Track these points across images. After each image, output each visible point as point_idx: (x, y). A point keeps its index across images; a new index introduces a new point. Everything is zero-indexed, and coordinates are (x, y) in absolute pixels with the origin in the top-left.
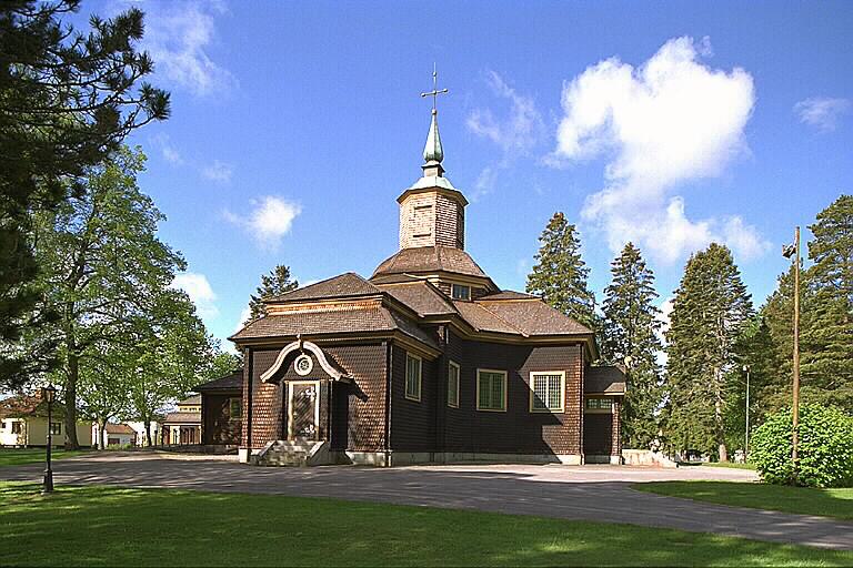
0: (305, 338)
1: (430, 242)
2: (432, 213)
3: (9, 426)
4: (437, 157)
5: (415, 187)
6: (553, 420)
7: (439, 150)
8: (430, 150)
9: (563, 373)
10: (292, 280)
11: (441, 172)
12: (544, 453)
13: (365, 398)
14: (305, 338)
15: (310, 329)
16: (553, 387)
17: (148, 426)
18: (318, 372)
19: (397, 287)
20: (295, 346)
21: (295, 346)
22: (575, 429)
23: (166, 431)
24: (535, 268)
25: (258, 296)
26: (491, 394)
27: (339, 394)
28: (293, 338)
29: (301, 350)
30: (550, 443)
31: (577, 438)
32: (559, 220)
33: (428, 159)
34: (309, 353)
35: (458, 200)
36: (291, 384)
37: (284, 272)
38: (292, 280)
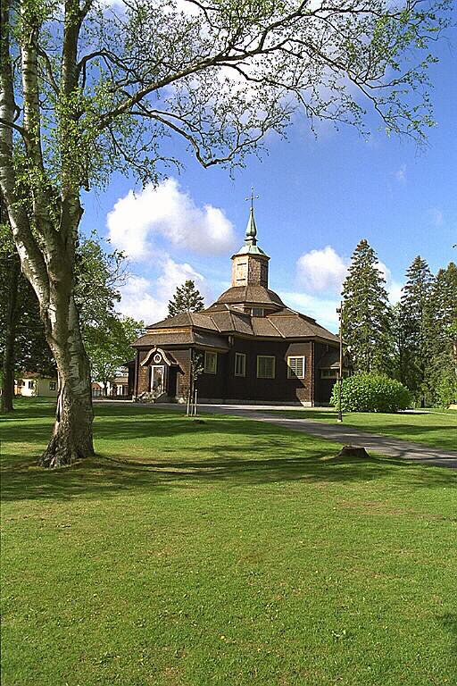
0: (158, 346)
1: (245, 283)
2: (246, 268)
3: (27, 384)
4: (253, 234)
5: (240, 253)
6: (300, 384)
7: (253, 230)
8: (248, 231)
9: (304, 357)
10: (195, 289)
11: (254, 242)
12: (297, 401)
13: (183, 374)
14: (158, 346)
15: (162, 342)
16: (299, 364)
17: (105, 384)
18: (163, 362)
19: (218, 314)
20: (153, 350)
21: (153, 350)
22: (309, 384)
23: (115, 388)
24: (348, 278)
25: (174, 301)
26: (264, 367)
27: (172, 372)
28: (153, 347)
29: (156, 352)
30: (298, 395)
31: (310, 393)
32: (364, 245)
33: (248, 235)
34: (160, 353)
35: (263, 260)
36: (153, 367)
37: (190, 285)
38: (195, 289)
